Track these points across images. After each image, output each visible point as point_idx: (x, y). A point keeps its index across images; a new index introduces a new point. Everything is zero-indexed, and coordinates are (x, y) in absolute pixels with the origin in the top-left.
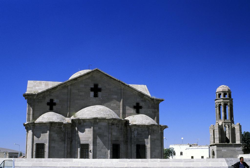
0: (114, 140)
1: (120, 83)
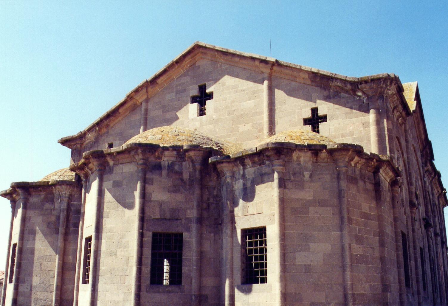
0: (158, 217)
1: (257, 63)
